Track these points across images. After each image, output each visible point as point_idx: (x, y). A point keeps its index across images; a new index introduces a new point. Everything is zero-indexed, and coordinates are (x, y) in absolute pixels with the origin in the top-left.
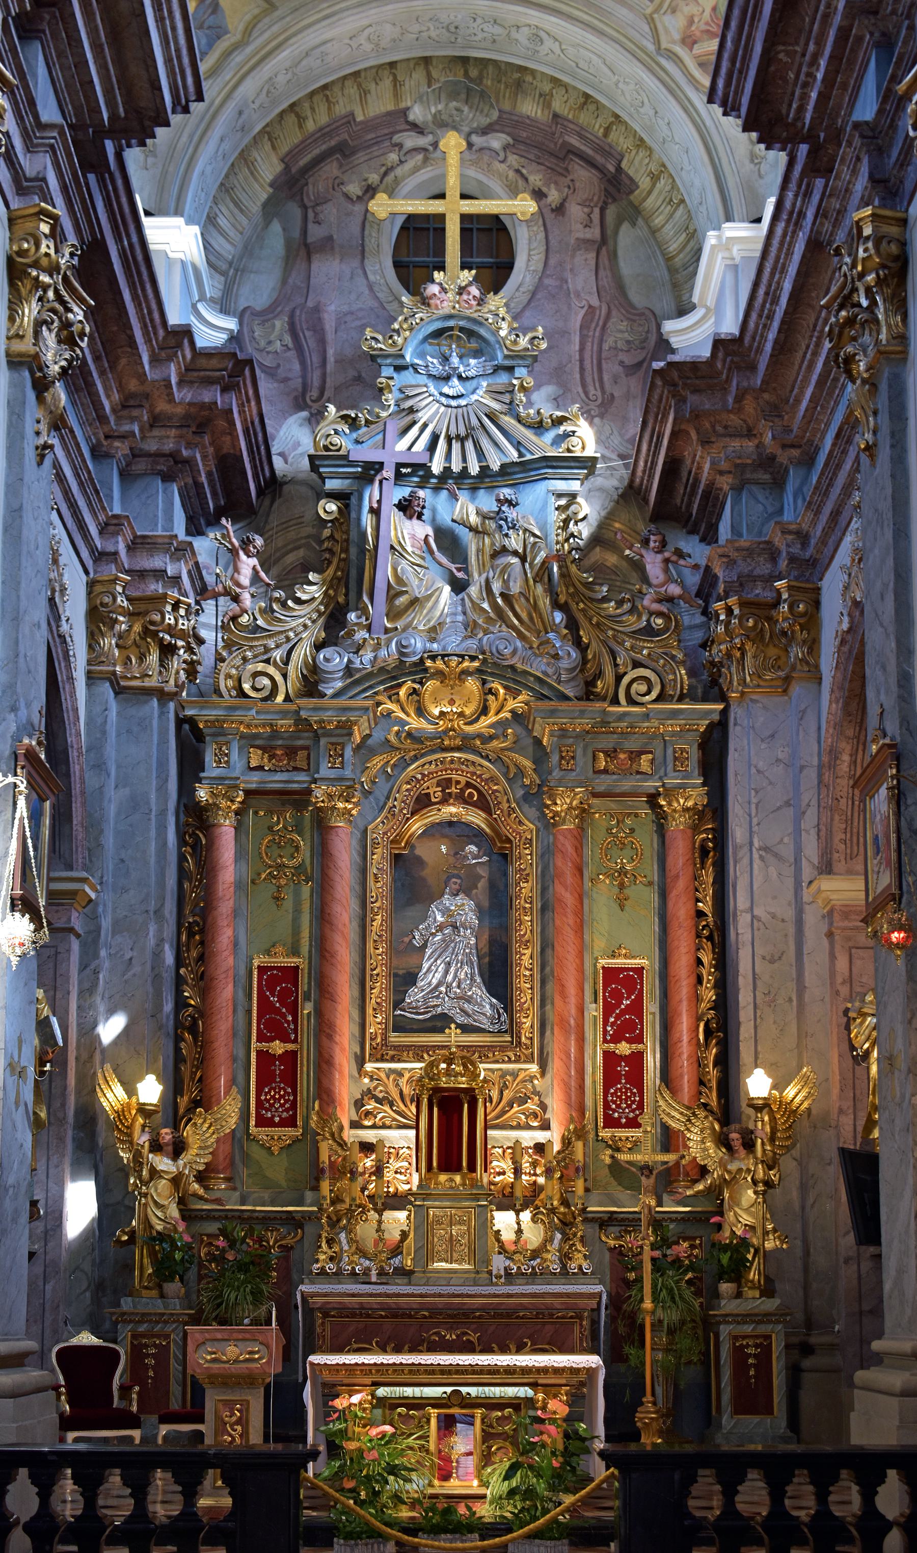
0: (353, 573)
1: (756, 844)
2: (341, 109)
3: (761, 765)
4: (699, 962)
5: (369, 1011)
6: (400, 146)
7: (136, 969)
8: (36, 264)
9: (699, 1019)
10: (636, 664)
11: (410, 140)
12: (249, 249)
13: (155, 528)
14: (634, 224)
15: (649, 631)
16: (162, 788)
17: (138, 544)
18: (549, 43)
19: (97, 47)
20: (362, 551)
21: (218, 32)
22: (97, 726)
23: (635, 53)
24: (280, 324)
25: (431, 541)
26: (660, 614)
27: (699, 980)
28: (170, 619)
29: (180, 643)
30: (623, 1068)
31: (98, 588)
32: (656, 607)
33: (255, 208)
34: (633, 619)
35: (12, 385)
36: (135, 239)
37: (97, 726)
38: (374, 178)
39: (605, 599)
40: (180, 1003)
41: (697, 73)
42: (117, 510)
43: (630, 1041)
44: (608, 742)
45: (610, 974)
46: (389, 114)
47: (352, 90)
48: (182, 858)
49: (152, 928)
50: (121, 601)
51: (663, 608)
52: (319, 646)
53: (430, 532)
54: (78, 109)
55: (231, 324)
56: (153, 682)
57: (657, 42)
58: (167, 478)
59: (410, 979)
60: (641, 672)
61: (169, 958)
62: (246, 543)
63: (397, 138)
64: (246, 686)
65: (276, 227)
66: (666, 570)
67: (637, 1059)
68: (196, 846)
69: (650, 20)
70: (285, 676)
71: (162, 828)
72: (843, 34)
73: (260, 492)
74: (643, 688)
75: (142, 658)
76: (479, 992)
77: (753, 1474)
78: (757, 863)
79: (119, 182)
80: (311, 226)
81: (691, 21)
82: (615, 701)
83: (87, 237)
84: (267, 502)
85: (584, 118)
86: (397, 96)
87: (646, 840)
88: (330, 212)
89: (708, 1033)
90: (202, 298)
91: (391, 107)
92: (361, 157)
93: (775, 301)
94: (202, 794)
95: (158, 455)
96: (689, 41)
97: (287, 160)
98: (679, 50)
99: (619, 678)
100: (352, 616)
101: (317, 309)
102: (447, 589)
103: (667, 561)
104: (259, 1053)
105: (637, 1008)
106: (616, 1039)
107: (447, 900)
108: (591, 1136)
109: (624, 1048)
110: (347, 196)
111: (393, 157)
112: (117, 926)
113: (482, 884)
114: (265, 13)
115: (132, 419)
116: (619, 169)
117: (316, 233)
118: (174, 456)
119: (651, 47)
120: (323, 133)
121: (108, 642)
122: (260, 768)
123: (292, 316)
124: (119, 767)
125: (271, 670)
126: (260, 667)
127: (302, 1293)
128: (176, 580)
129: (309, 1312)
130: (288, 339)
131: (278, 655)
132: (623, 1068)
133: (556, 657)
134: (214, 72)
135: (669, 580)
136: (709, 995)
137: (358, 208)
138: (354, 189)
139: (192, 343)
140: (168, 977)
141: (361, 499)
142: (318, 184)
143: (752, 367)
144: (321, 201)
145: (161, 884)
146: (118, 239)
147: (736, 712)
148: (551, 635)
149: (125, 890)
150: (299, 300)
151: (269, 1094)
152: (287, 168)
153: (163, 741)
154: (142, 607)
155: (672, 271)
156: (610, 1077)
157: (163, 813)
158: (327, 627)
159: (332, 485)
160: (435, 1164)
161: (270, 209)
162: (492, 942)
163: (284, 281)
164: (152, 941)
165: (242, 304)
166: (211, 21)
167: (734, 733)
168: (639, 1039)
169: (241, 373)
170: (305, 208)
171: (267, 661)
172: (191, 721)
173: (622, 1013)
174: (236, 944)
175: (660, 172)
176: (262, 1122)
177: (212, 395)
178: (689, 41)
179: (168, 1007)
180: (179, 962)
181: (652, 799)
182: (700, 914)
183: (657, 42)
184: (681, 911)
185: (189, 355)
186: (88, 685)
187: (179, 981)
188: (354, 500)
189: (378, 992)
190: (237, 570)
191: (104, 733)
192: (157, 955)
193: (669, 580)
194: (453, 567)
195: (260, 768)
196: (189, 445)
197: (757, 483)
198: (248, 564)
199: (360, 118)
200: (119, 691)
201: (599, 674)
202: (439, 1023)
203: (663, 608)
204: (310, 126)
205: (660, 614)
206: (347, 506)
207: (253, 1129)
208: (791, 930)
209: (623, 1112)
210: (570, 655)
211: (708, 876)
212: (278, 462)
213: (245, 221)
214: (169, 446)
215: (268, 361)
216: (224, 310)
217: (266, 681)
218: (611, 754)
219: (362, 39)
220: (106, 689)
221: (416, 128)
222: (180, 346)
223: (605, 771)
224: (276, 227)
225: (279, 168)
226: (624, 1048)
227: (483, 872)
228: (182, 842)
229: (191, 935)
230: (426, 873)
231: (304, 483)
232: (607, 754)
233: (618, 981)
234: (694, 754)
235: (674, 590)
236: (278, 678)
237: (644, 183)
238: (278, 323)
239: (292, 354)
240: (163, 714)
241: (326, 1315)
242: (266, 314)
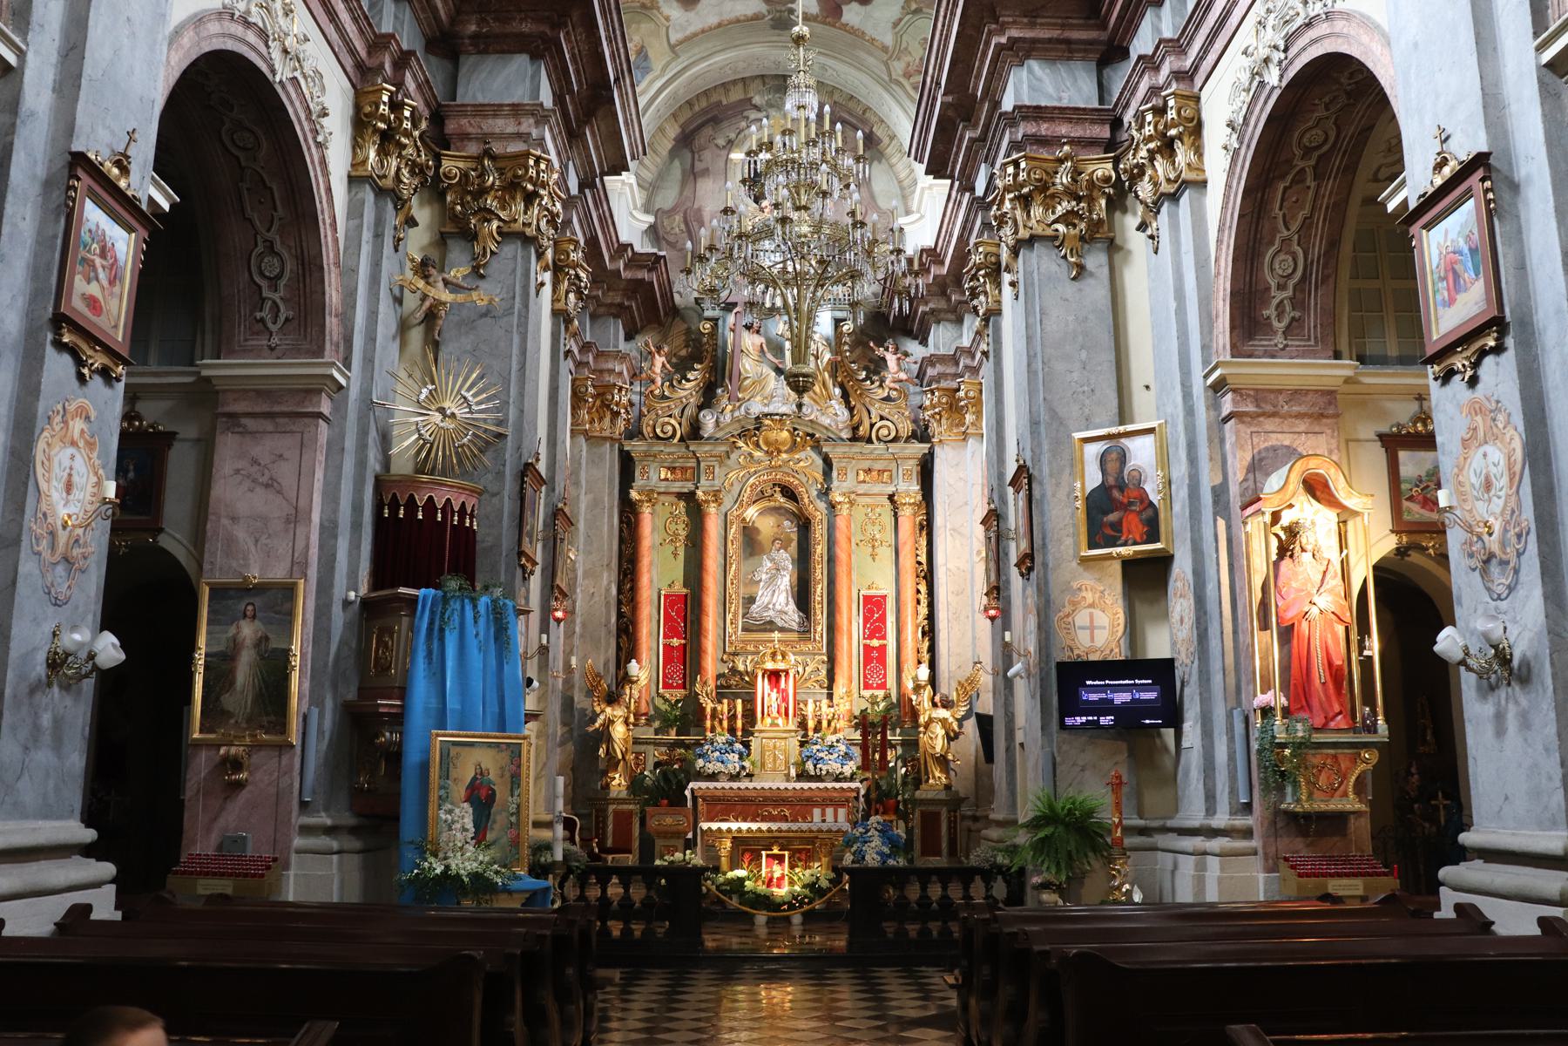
0: (720, 364)
1: (948, 526)
2: (714, 99)
3: (952, 482)
4: (918, 592)
5: (728, 621)
6: (747, 118)
7: (596, 599)
8: (568, 266)
9: (917, 627)
10: (882, 418)
11: (753, 115)
12: (661, 176)
13: (608, 346)
14: (880, 162)
15: (888, 399)
16: (610, 494)
17: (600, 355)
18: (830, 71)
19: (597, 148)
20: (725, 352)
21: (647, 70)
22: (576, 460)
23: (879, 80)
24: (678, 218)
25: (764, 346)
26: (895, 389)
27: (918, 602)
28: (617, 398)
29: (542, 192)
30: (875, 654)
31: (578, 383)
32: (892, 385)
33: (665, 153)
34: (880, 391)
35: (553, 324)
36: (606, 208)
37: (576, 460)
38: (733, 136)
39: (864, 380)
40: (620, 615)
41: (912, 92)
42: (588, 339)
43: (879, 638)
44: (866, 464)
45: (868, 599)
46: (741, 101)
47: (722, 91)
48: (621, 530)
49: (605, 575)
50: (591, 390)
51: (896, 386)
52: (700, 408)
53: (763, 340)
54: (585, 173)
55: (651, 219)
56: (607, 434)
57: (890, 75)
58: (616, 316)
59: (751, 600)
60: (884, 422)
61: (614, 591)
62: (659, 349)
63: (745, 114)
64: (658, 431)
65: (677, 163)
66: (899, 365)
67: (883, 649)
68: (629, 523)
69: (886, 64)
70: (680, 424)
71: (611, 517)
72: (969, 148)
73: (666, 314)
74: (886, 432)
75: (601, 419)
76: (792, 607)
77: (934, 878)
78: (949, 537)
79: (602, 193)
80: (697, 163)
81: (908, 65)
82: (869, 441)
83: (588, 235)
84: (670, 320)
85: (851, 105)
86: (745, 92)
87: (888, 519)
88: (707, 155)
89: (924, 634)
90: (635, 208)
91: (742, 97)
92: (725, 124)
93: (951, 236)
94: (634, 495)
95: (611, 305)
96: (907, 75)
97: (683, 127)
98: (901, 80)
99: (872, 426)
100: (719, 391)
101: (699, 210)
102: (773, 374)
103: (899, 359)
104: (665, 645)
105: (883, 619)
106: (871, 637)
107: (774, 554)
108: (856, 695)
109: (875, 643)
110: (717, 146)
111: (743, 124)
112: (586, 574)
113: (794, 544)
114: (673, 60)
115: (598, 289)
116: (871, 132)
117: (699, 166)
118: (621, 305)
119: (887, 78)
120: (704, 111)
121: (584, 414)
122: (666, 479)
123: (685, 213)
124: (587, 482)
125: (673, 421)
126: (667, 419)
127: (692, 790)
128: (621, 374)
129: (694, 798)
130: (683, 226)
131: (677, 412)
132: (875, 654)
133: (836, 414)
134: (643, 92)
135: (900, 369)
136: (923, 610)
137: (724, 153)
138: (721, 142)
139: (632, 249)
140: (613, 602)
141: (724, 321)
142: (701, 139)
143: (942, 263)
144: (702, 149)
145: (610, 549)
146: (597, 208)
147: (937, 450)
148: (833, 402)
149: (590, 553)
150: (689, 204)
151: (669, 668)
152: (683, 131)
153: (611, 467)
154: (601, 390)
155: (902, 189)
156: (868, 660)
157: (611, 508)
158: (704, 394)
159: (708, 313)
160: (620, 807)
161: (673, 153)
162: (800, 579)
163: (681, 193)
164: (605, 582)
165: (657, 207)
166: (644, 64)
167: (937, 462)
168: (884, 637)
169: (659, 262)
170: (693, 152)
171: (670, 416)
172: (628, 453)
173: (875, 621)
174: (651, 581)
175: (892, 137)
176: (666, 686)
177: (643, 275)
178: (907, 75)
179: (614, 619)
180: (620, 591)
181: (891, 497)
182: (919, 563)
183: (890, 75)
184: (908, 563)
185: (630, 254)
186: (572, 437)
187: (619, 603)
188: (720, 322)
189: (735, 607)
190: (653, 364)
191: (580, 464)
192: (608, 590)
193: (900, 369)
194: (776, 361)
195: (666, 479)
196: (629, 299)
197: (947, 320)
198: (659, 360)
199: (725, 102)
200: (588, 438)
201: (860, 423)
202: (770, 626)
203: (896, 386)
204: (697, 108)
205: (895, 389)
206: (716, 325)
207: (661, 691)
208: (969, 576)
209: (875, 681)
210: (843, 414)
211: (924, 542)
212: (677, 297)
213: (659, 160)
214: (618, 300)
215: (671, 239)
216: (647, 211)
217: (670, 428)
218: (868, 471)
219: (727, 69)
220: (582, 439)
221: (757, 108)
222: (626, 251)
223: (864, 482)
224: (677, 163)
225: (678, 130)
226: (875, 643)
227: (795, 537)
228: (621, 522)
229: (625, 575)
230: (760, 538)
231: (691, 309)
232: (865, 471)
233: (872, 603)
234: (916, 469)
235: (903, 376)
236: (677, 426)
237: (886, 140)
238: (677, 217)
239: (686, 235)
240: (612, 450)
241: (704, 800)
242: (670, 213)
